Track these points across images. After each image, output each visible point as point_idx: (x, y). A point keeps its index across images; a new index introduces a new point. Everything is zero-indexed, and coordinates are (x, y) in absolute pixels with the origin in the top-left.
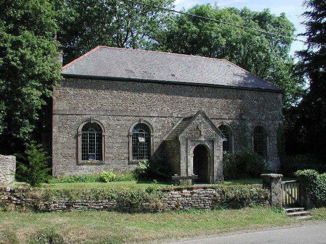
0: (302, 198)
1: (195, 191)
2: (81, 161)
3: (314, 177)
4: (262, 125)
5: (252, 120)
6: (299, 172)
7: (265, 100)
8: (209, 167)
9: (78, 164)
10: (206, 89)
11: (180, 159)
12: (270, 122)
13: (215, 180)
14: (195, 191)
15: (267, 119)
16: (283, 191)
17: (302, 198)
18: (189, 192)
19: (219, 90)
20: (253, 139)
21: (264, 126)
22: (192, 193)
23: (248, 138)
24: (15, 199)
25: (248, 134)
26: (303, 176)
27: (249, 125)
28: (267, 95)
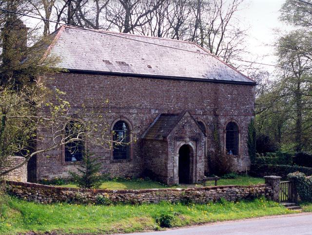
0: (294, 195)
1: (224, 189)
2: (64, 162)
3: (304, 179)
4: (234, 121)
5: (225, 116)
6: (293, 174)
7: (239, 94)
8: (191, 168)
9: (62, 164)
10: (182, 82)
11: (167, 159)
12: (243, 117)
13: (197, 180)
14: (224, 189)
15: (239, 115)
16: (282, 188)
17: (294, 195)
18: (221, 190)
19: (194, 83)
20: (225, 137)
21: (236, 122)
22: (223, 191)
23: (221, 135)
24: (120, 198)
25: (221, 131)
26: (294, 178)
27: (222, 121)
28: (241, 88)
